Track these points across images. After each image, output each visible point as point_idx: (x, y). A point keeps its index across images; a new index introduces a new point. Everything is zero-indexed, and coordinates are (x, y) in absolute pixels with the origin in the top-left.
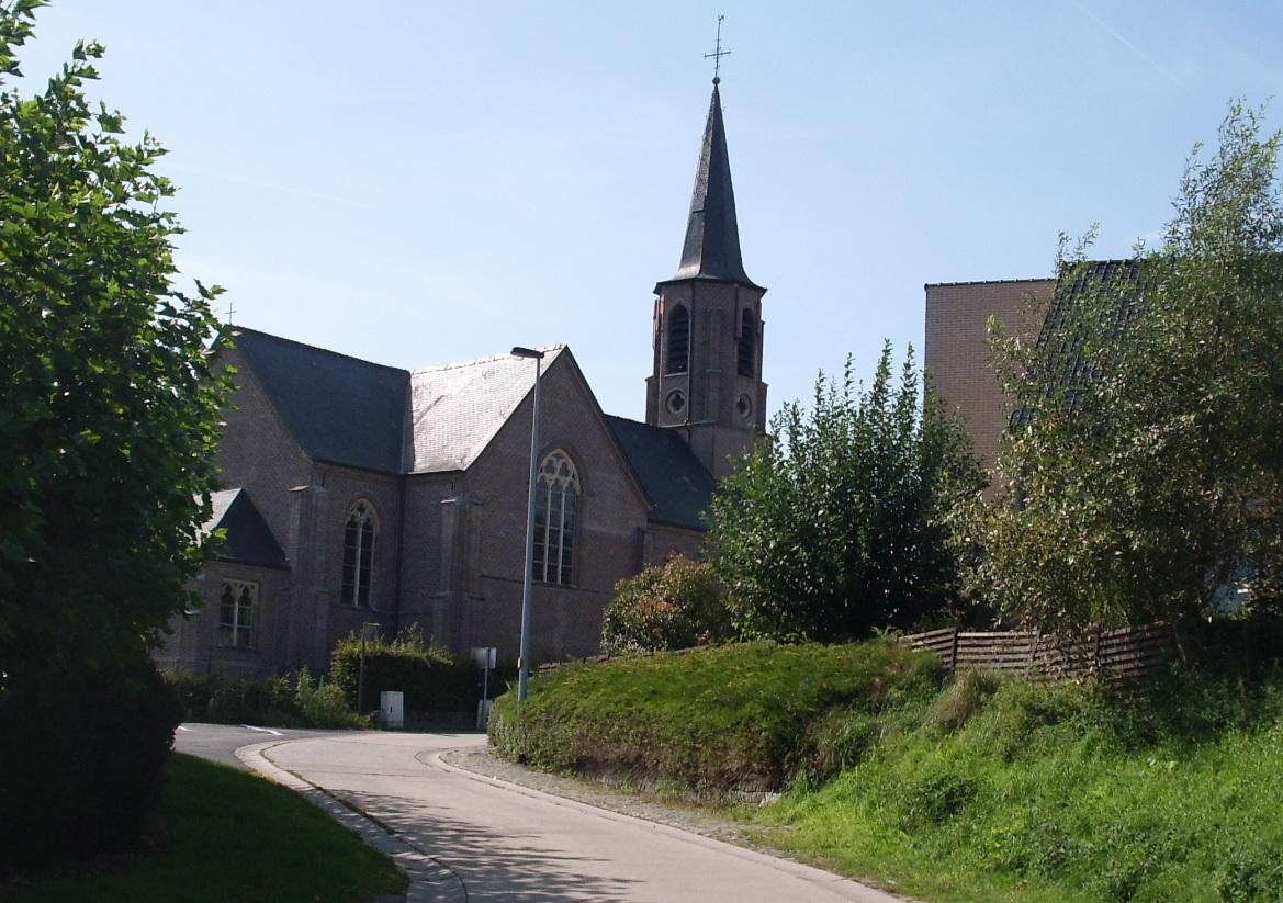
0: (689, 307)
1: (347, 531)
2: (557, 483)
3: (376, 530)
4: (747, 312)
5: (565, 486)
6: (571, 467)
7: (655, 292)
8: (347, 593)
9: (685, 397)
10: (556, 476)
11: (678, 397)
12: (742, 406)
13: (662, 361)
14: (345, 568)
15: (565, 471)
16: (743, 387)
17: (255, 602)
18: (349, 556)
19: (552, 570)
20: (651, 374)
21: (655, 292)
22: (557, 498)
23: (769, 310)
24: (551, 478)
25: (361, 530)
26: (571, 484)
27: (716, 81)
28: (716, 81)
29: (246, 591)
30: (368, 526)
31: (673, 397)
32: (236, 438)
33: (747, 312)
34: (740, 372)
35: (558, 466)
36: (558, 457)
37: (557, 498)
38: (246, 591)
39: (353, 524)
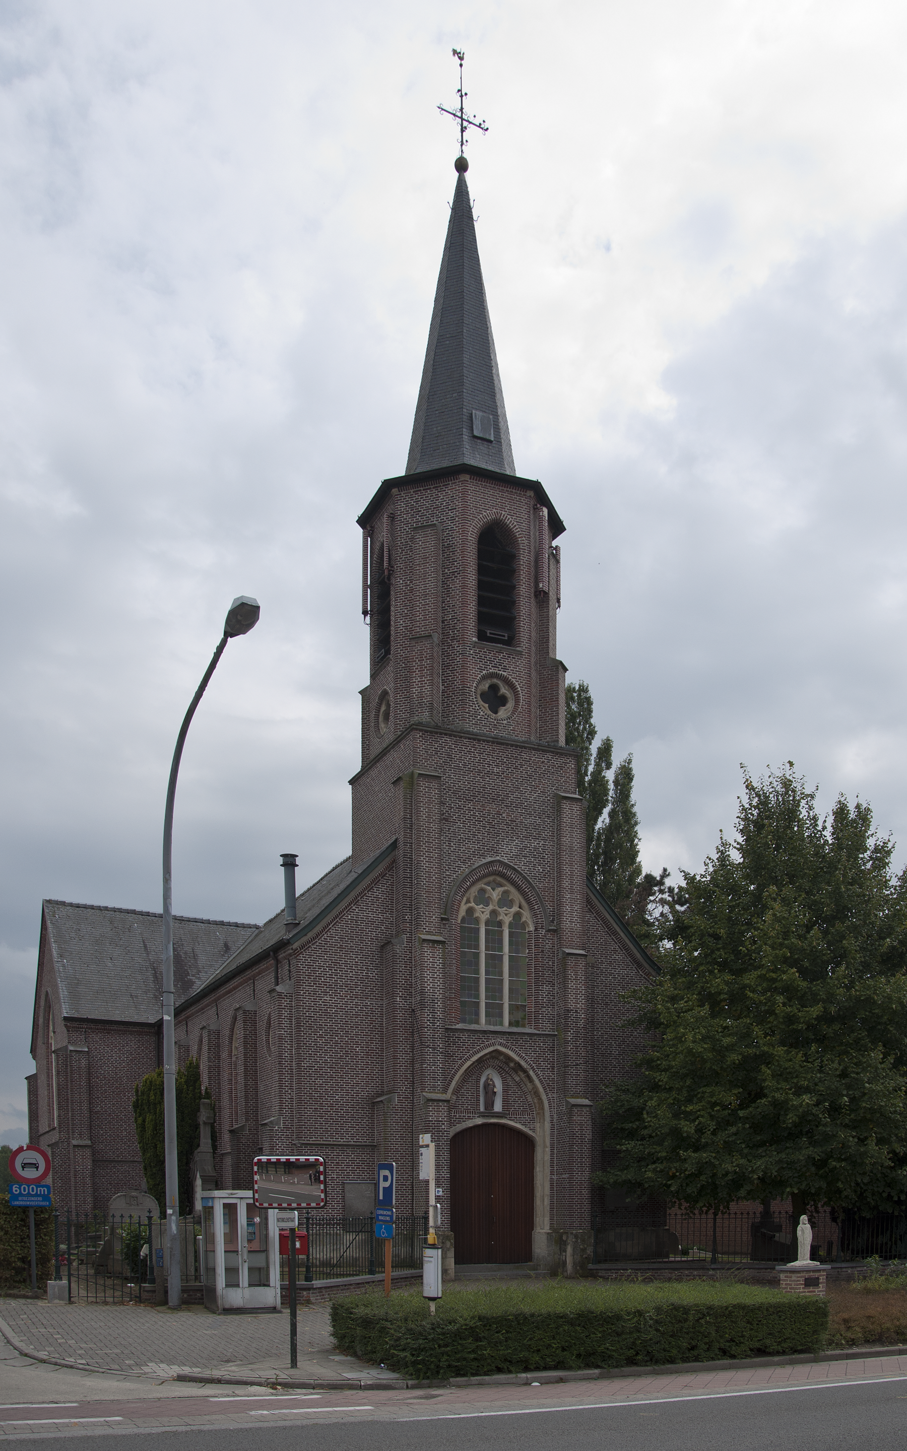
6: (515, 895)
27: (461, 166)
28: (461, 166)
35: (495, 895)
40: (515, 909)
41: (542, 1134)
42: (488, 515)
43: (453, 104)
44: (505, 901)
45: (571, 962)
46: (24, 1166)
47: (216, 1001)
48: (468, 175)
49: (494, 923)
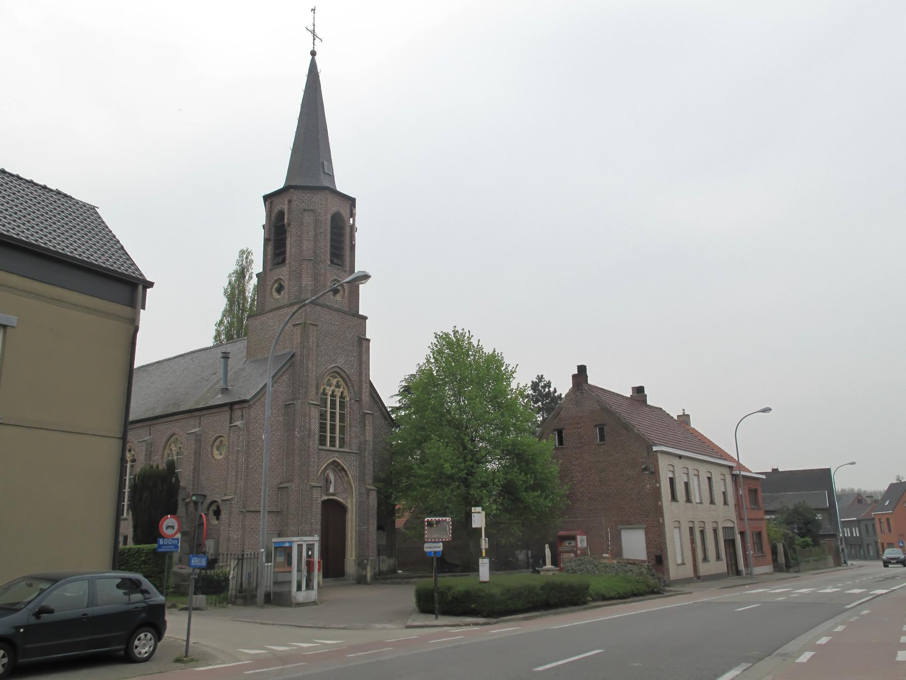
6: (342, 382)
27: (313, 53)
28: (313, 53)
35: (334, 382)
40: (341, 390)
41: (351, 504)
42: (334, 210)
43: (311, 28)
44: (338, 386)
45: (367, 417)
46: (168, 527)
47: (150, 426)
48: (316, 58)
49: (333, 395)
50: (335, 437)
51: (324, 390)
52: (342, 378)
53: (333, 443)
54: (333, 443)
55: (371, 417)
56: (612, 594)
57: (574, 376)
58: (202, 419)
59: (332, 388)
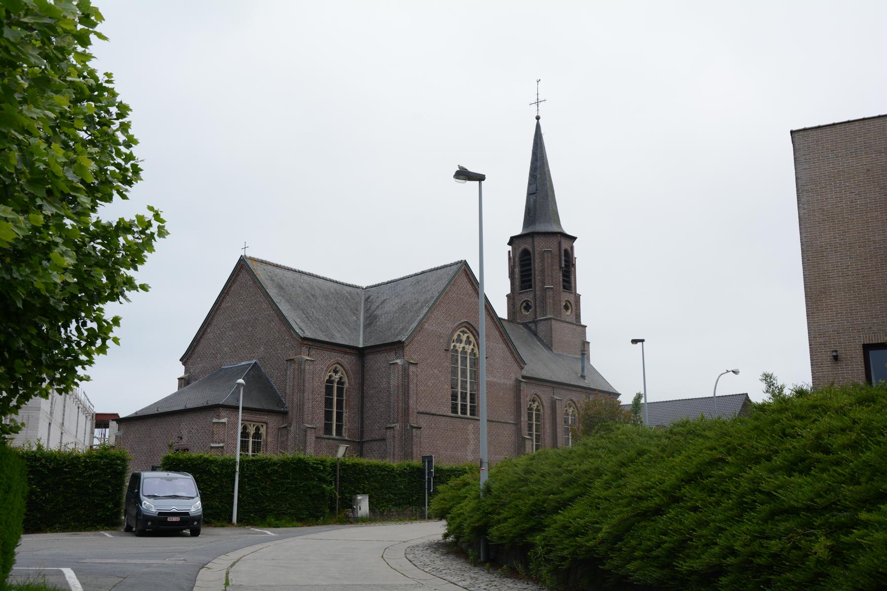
0: (530, 249)
1: (327, 386)
2: (464, 352)
3: (346, 385)
4: (566, 251)
5: (469, 351)
6: (472, 339)
7: (509, 244)
8: (328, 429)
9: (532, 304)
10: (462, 345)
11: (527, 304)
12: (566, 308)
13: (517, 283)
14: (326, 411)
15: (468, 342)
16: (566, 296)
17: (264, 436)
18: (328, 403)
19: (464, 407)
20: (509, 292)
21: (509, 244)
22: (464, 359)
23: (578, 250)
24: (460, 347)
25: (335, 385)
26: (473, 350)
27: (538, 118)
28: (538, 118)
29: (258, 429)
30: (340, 382)
31: (524, 304)
32: (250, 329)
33: (566, 251)
34: (564, 287)
35: (464, 338)
36: (464, 332)
37: (464, 359)
38: (258, 429)
39: (330, 381)
50: (466, 405)
51: (455, 346)
52: (471, 332)
53: (464, 411)
54: (464, 411)
55: (549, 255)
56: (366, 422)
57: (117, 415)
58: (514, 427)
59: (462, 345)
